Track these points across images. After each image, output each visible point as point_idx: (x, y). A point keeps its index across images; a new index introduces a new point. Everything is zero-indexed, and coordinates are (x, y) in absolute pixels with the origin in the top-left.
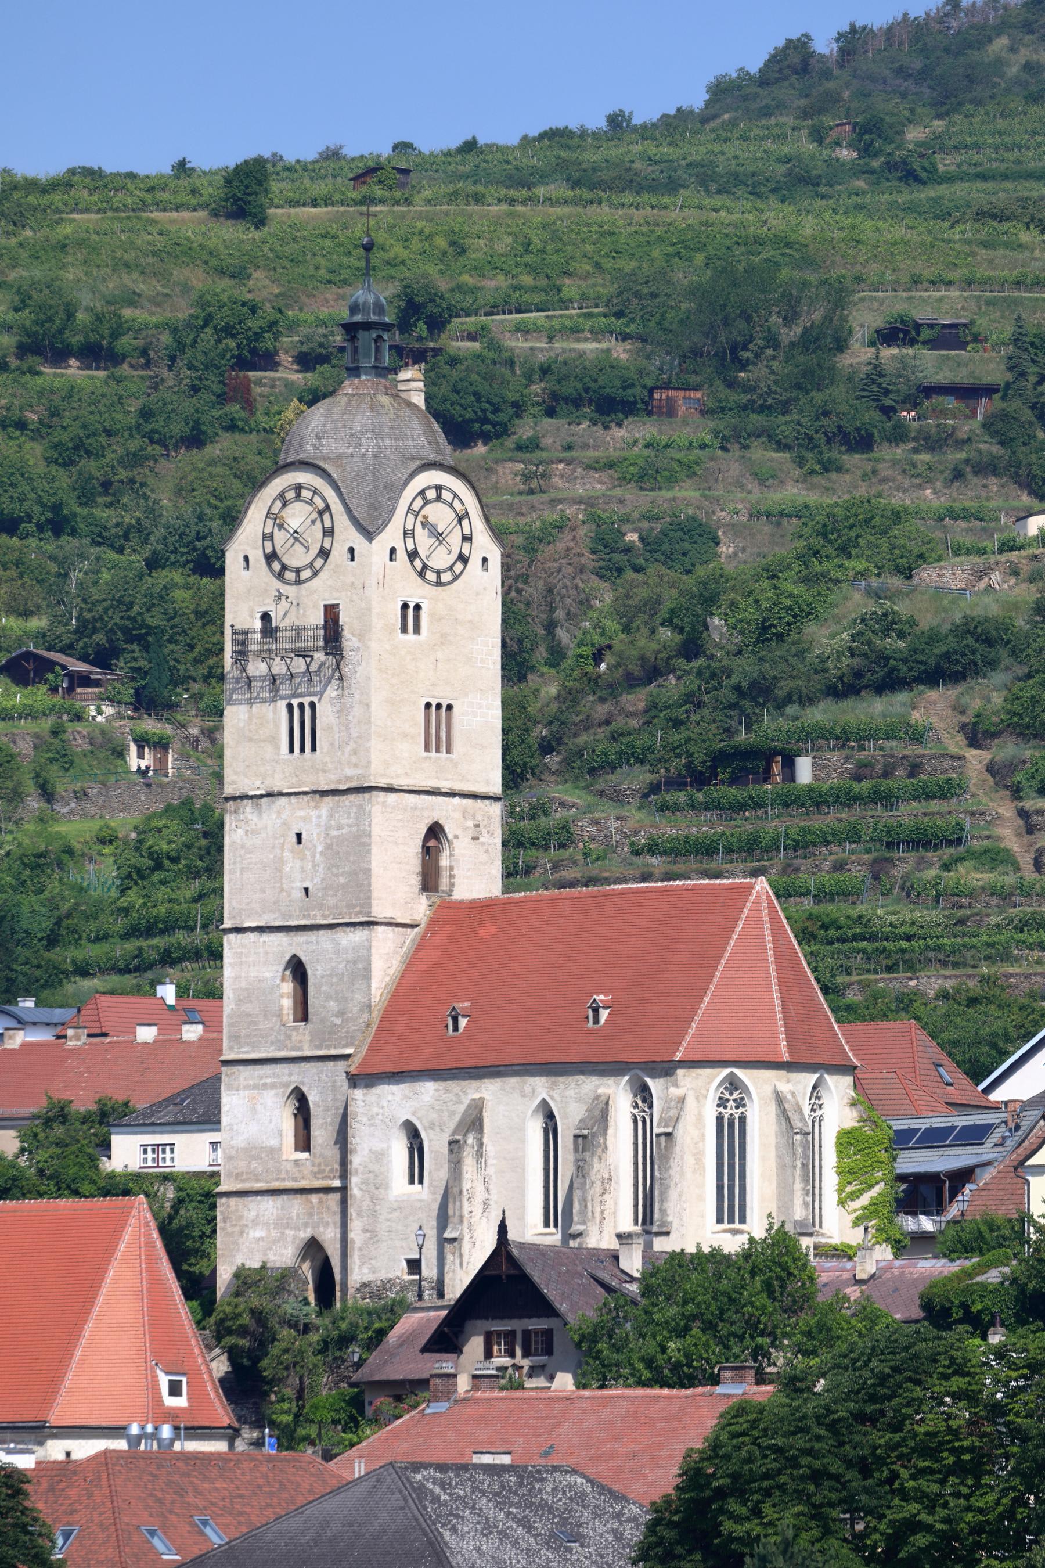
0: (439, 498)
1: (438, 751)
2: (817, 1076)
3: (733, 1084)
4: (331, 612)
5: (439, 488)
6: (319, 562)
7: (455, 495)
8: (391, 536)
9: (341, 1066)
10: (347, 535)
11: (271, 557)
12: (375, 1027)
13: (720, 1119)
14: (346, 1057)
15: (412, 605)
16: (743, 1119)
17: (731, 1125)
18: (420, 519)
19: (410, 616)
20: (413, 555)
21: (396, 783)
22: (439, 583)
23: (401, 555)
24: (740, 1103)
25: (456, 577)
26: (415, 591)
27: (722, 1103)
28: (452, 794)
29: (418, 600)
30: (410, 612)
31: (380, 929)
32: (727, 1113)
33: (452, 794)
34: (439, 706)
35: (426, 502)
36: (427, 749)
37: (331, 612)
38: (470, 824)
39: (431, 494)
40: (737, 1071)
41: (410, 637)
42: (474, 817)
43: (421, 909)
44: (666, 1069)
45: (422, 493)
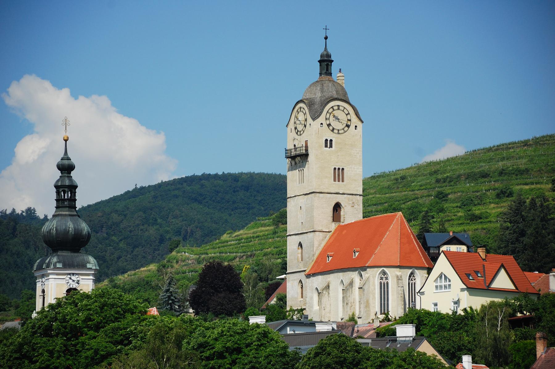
0: (339, 109)
1: (339, 181)
2: (411, 270)
3: (384, 273)
4: (306, 141)
5: (339, 106)
6: (346, 128)
7: (344, 108)
8: (322, 119)
9: (303, 273)
10: (310, 120)
11: (296, 128)
12: (314, 261)
13: (381, 283)
14: (305, 271)
15: (329, 140)
16: (387, 283)
17: (412, 284)
18: (332, 115)
19: (328, 143)
20: (329, 125)
21: (345, 192)
22: (338, 133)
23: (325, 125)
24: (387, 278)
25: (345, 132)
26: (330, 136)
27: (382, 278)
28: (343, 194)
29: (331, 138)
30: (329, 142)
31: (317, 233)
32: (382, 281)
33: (343, 194)
34: (339, 169)
35: (334, 110)
36: (335, 180)
37: (306, 141)
38: (351, 202)
39: (336, 108)
40: (385, 269)
41: (327, 149)
42: (352, 200)
43: (333, 226)
44: (364, 269)
45: (332, 107)
